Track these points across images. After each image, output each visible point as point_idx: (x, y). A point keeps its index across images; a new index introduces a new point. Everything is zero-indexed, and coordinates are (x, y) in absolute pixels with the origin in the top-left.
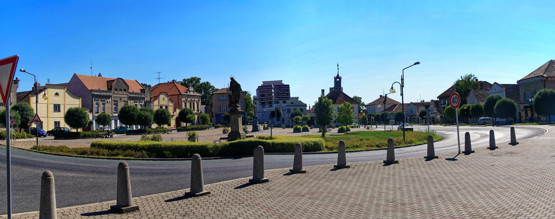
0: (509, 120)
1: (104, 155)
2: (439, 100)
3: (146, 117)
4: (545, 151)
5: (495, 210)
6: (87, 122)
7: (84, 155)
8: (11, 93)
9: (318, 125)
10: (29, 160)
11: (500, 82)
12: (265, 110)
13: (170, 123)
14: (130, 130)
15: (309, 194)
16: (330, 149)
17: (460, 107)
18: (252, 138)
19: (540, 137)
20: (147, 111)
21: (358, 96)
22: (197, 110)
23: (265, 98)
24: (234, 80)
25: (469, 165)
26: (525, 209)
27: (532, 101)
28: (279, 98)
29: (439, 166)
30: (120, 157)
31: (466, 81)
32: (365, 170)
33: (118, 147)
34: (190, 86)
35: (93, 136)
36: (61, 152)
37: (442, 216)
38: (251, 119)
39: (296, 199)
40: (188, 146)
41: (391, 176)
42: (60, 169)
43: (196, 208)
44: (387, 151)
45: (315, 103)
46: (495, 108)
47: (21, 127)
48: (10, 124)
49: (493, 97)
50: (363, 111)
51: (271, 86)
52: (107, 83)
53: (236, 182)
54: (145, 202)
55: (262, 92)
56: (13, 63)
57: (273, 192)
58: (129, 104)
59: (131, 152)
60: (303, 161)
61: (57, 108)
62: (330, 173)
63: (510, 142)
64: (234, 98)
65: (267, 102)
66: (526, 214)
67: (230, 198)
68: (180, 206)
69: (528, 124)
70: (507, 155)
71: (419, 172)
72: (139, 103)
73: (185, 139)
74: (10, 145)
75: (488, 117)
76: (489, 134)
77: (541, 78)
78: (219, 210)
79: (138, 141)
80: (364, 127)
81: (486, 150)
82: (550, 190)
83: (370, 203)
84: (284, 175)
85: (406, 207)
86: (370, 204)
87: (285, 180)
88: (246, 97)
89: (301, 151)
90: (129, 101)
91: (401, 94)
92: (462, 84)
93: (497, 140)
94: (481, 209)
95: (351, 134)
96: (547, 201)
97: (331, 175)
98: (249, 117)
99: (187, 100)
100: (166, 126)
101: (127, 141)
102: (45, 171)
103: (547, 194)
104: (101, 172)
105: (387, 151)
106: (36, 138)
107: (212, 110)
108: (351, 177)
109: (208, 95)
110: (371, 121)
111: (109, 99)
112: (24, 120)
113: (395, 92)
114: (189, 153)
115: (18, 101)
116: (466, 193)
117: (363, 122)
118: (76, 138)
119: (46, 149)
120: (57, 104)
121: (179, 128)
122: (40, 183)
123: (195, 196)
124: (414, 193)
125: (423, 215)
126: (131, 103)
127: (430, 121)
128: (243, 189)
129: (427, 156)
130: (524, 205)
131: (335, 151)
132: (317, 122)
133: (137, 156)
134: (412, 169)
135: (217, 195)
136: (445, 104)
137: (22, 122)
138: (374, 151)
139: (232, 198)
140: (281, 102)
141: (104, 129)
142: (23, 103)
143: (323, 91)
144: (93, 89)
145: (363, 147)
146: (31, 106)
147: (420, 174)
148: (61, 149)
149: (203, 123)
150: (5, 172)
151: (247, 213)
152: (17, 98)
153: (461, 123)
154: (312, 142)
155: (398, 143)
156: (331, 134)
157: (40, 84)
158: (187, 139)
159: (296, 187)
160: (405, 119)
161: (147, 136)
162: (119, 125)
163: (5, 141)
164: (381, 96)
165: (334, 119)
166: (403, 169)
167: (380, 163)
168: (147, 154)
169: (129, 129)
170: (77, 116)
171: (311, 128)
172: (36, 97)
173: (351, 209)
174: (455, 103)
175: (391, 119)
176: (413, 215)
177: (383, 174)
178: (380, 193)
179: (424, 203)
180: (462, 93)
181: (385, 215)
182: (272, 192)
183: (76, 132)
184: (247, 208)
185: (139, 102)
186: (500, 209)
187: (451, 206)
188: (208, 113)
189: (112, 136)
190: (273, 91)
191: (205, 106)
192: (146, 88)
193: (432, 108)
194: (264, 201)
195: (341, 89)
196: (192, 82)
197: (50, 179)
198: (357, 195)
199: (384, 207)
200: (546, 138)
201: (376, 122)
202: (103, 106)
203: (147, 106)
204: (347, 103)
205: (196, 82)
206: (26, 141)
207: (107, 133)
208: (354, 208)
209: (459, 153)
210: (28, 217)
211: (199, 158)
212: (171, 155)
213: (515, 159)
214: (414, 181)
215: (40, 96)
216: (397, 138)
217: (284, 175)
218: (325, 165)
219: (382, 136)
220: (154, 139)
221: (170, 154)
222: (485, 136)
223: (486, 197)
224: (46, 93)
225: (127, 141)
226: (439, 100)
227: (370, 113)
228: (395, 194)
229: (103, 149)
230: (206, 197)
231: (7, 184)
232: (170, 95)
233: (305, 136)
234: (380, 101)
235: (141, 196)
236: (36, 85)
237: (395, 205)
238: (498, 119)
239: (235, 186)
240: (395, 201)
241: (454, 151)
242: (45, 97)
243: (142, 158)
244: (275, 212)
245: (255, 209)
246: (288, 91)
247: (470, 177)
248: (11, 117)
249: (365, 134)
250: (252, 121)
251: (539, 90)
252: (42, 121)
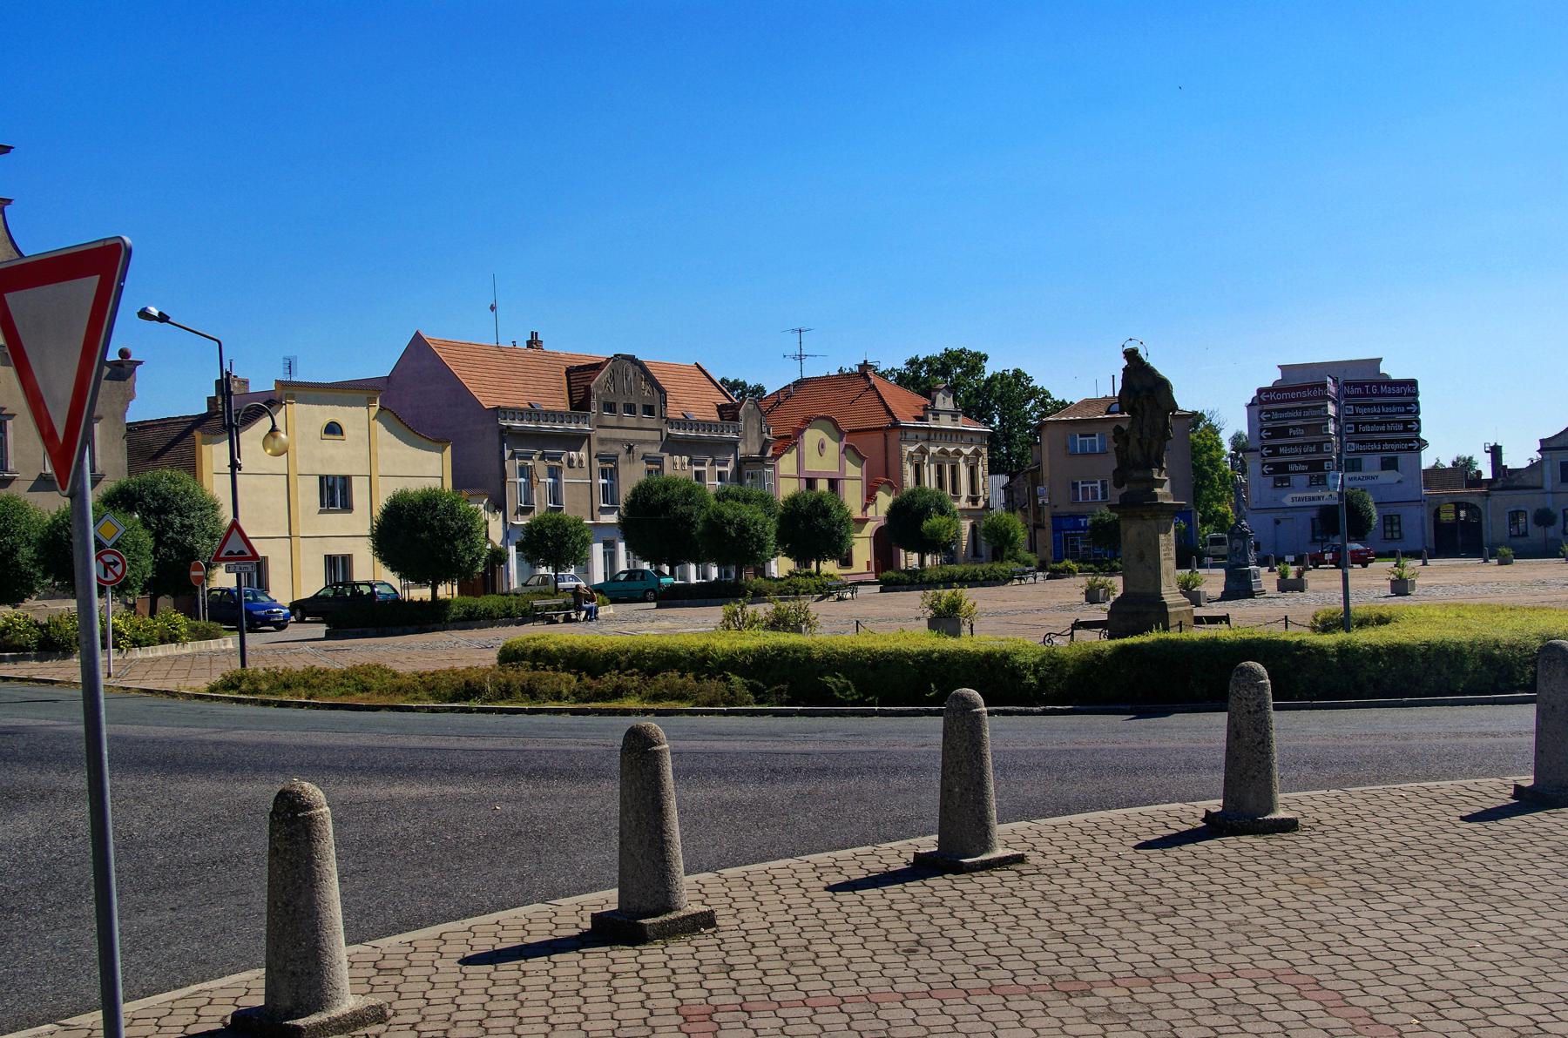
1: (558, 697)
3: (743, 528)
6: (479, 556)
7: (467, 700)
8: (97, 427)
10: (202, 743)
12: (1287, 501)
13: (850, 554)
14: (672, 585)
18: (1224, 626)
20: (747, 500)
22: (969, 499)
23: (1288, 446)
24: (1140, 360)
28: (1362, 443)
30: (631, 703)
33: (623, 658)
34: (939, 390)
35: (507, 616)
36: (363, 691)
38: (1216, 541)
40: (927, 655)
42: (359, 768)
43: (962, 920)
47: (155, 588)
48: (98, 578)
51: (1324, 386)
52: (568, 380)
53: (1145, 821)
54: (740, 893)
55: (1276, 415)
56: (99, 276)
58: (668, 471)
59: (680, 681)
61: (335, 494)
64: (1139, 441)
65: (1297, 463)
67: (1112, 887)
68: (891, 909)
72: (713, 464)
73: (914, 622)
74: (103, 680)
78: (1064, 936)
79: (709, 635)
88: (1199, 437)
90: (667, 460)
98: (1208, 532)
99: (923, 451)
100: (830, 567)
101: (660, 632)
102: (286, 786)
104: (545, 770)
106: (237, 635)
107: (1036, 497)
109: (1019, 432)
111: (577, 450)
112: (171, 556)
114: (933, 686)
115: (133, 467)
118: (430, 628)
119: (287, 687)
120: (334, 477)
121: (890, 574)
122: (262, 842)
123: (959, 869)
126: (677, 467)
128: (1174, 852)
133: (703, 697)
135: (1056, 871)
137: (159, 566)
139: (1125, 888)
140: (1371, 462)
141: (556, 582)
142: (164, 475)
144: (502, 404)
146: (206, 485)
148: (359, 679)
149: (997, 556)
150: (80, 814)
152: (130, 452)
157: (246, 382)
158: (925, 622)
161: (750, 609)
162: (622, 565)
163: (75, 661)
168: (748, 689)
169: (670, 580)
170: (431, 528)
172: (227, 442)
183: (430, 599)
185: (710, 460)
188: (1018, 512)
189: (592, 614)
190: (1332, 410)
191: (1004, 479)
192: (745, 399)
196: (950, 373)
197: (310, 818)
202: (551, 480)
203: (748, 481)
205: (965, 374)
206: (187, 655)
207: (572, 600)
210: (209, 1004)
211: (976, 706)
212: (853, 690)
215: (252, 437)
220: (780, 622)
221: (850, 689)
224: (280, 425)
225: (660, 635)
229: (555, 669)
230: (1009, 875)
231: (91, 866)
232: (851, 432)
235: (724, 868)
236: (228, 386)
239: (1136, 836)
242: (277, 444)
243: (729, 704)
246: (1409, 412)
248: (100, 545)
250: (1224, 550)
252: (265, 558)
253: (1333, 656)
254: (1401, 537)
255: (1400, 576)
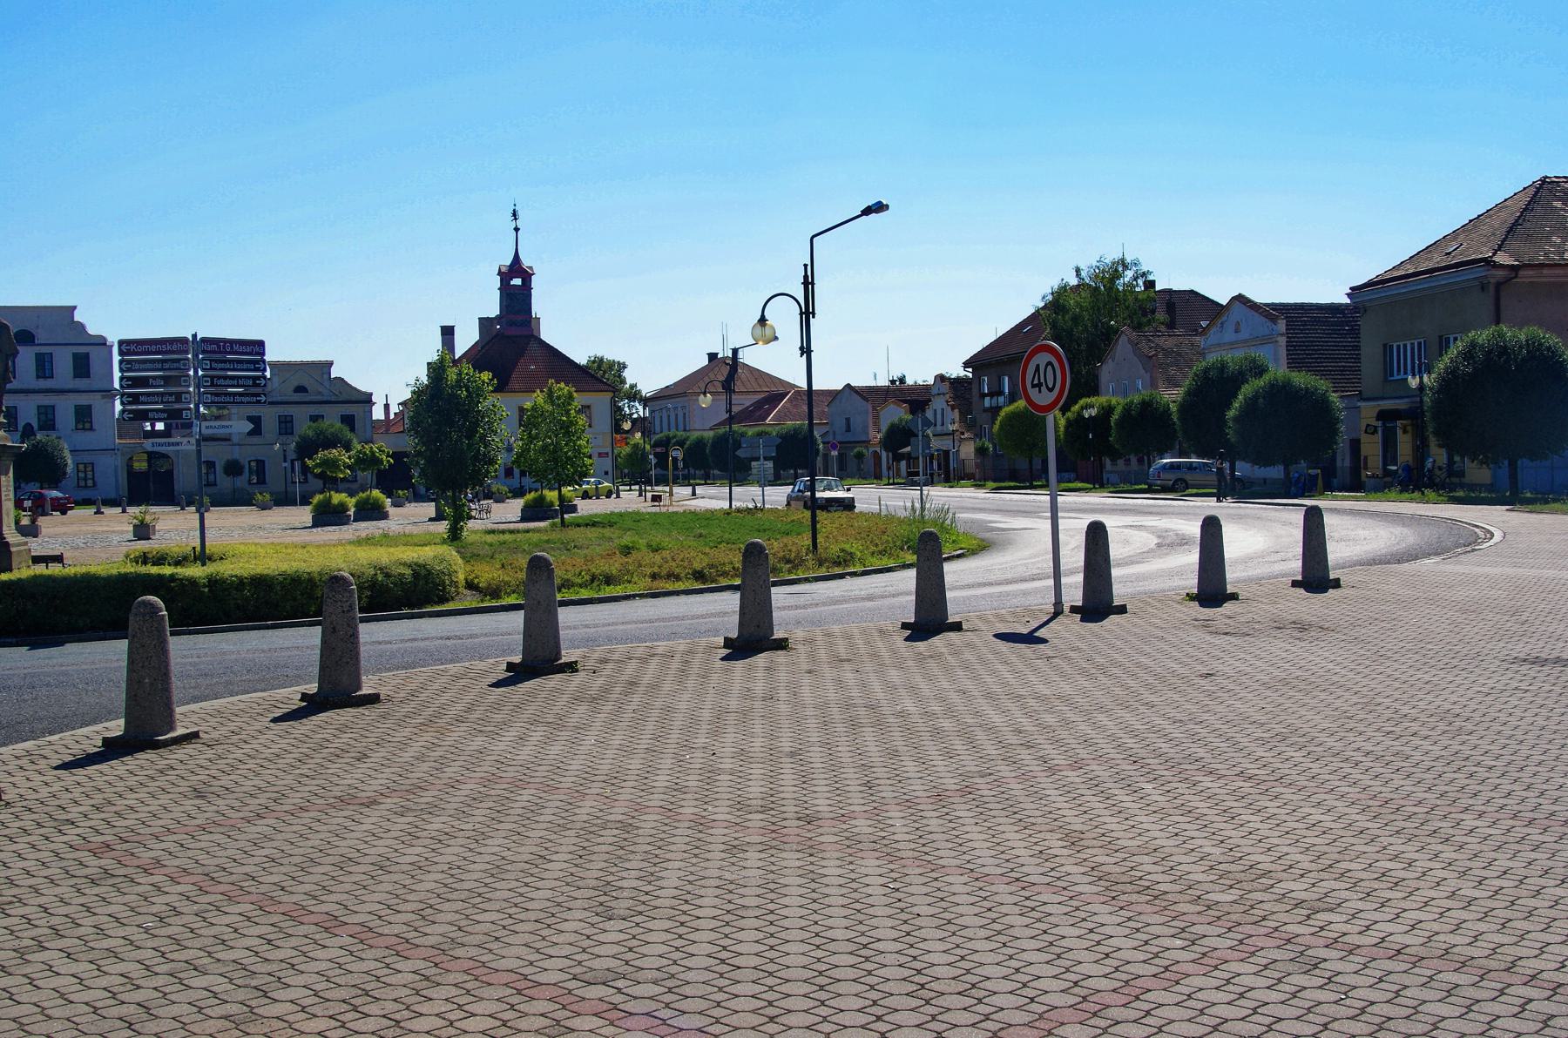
0: (1296, 475)
2: (970, 375)
4: (1476, 630)
5: (1211, 868)
9: (427, 490)
11: (1261, 296)
15: (399, 794)
16: (485, 595)
17: (1064, 410)
19: (1460, 563)
21: (609, 355)
25: (1099, 667)
26: (1355, 885)
27: (1421, 387)
28: (217, 395)
29: (966, 666)
31: (1097, 289)
32: (646, 679)
37: (975, 875)
39: (338, 818)
41: (758, 704)
44: (737, 596)
45: (411, 389)
46: (1231, 413)
49: (1223, 367)
50: (634, 422)
57: (227, 802)
60: (364, 651)
62: (491, 698)
63: (1299, 578)
66: (1360, 905)
69: (1393, 495)
70: (1277, 633)
71: (876, 686)
75: (1198, 457)
76: (1199, 535)
77: (1480, 272)
80: (640, 495)
81: (1178, 606)
82: (1488, 819)
83: (668, 817)
84: (275, 720)
85: (820, 831)
86: (666, 821)
87: (283, 744)
89: (351, 608)
91: (801, 348)
92: (1078, 304)
93: (1236, 562)
94: (1146, 859)
95: (579, 526)
96: (1468, 864)
97: (497, 706)
103: (1471, 831)
105: (737, 596)
108: (582, 708)
110: (667, 469)
113: (776, 338)
116: (1083, 786)
117: (635, 472)
123: (156, 746)
124: (857, 776)
125: (892, 866)
127: (932, 468)
129: (912, 621)
130: (1353, 866)
131: (512, 600)
132: (423, 474)
134: (849, 677)
136: (1001, 393)
138: (683, 599)
143: (448, 332)
145: (635, 579)
147: (881, 696)
151: (95, 914)
153: (1070, 481)
154: (405, 564)
155: (788, 561)
156: (491, 526)
159: (333, 768)
160: (819, 459)
164: (712, 357)
165: (502, 459)
166: (810, 672)
167: (711, 649)
171: (395, 505)
173: (586, 844)
174: (1044, 388)
175: (757, 459)
176: (851, 863)
177: (725, 693)
178: (709, 775)
179: (895, 815)
180: (1079, 345)
181: (733, 864)
182: (220, 802)
184: (96, 890)
186: (1233, 867)
187: (1012, 835)
193: (939, 412)
194: (182, 845)
195: (533, 322)
198: (613, 784)
199: (726, 831)
200: (1487, 570)
201: (692, 471)
204: (563, 388)
208: (600, 840)
209: (1058, 612)
213: (1320, 656)
214: (854, 725)
216: (785, 541)
217: (275, 720)
218: (467, 664)
219: (718, 532)
222: (1173, 543)
223: (1171, 812)
226: (970, 375)
227: (666, 433)
228: (773, 777)
233: (368, 541)
234: (707, 380)
237: (773, 824)
238: (1243, 469)
240: (772, 806)
241: (1033, 601)
244: (242, 888)
245: (140, 889)
247: (1102, 718)
249: (642, 524)
251: (1466, 330)
253: (205, 586)
254: (95, 485)
255: (142, 522)
